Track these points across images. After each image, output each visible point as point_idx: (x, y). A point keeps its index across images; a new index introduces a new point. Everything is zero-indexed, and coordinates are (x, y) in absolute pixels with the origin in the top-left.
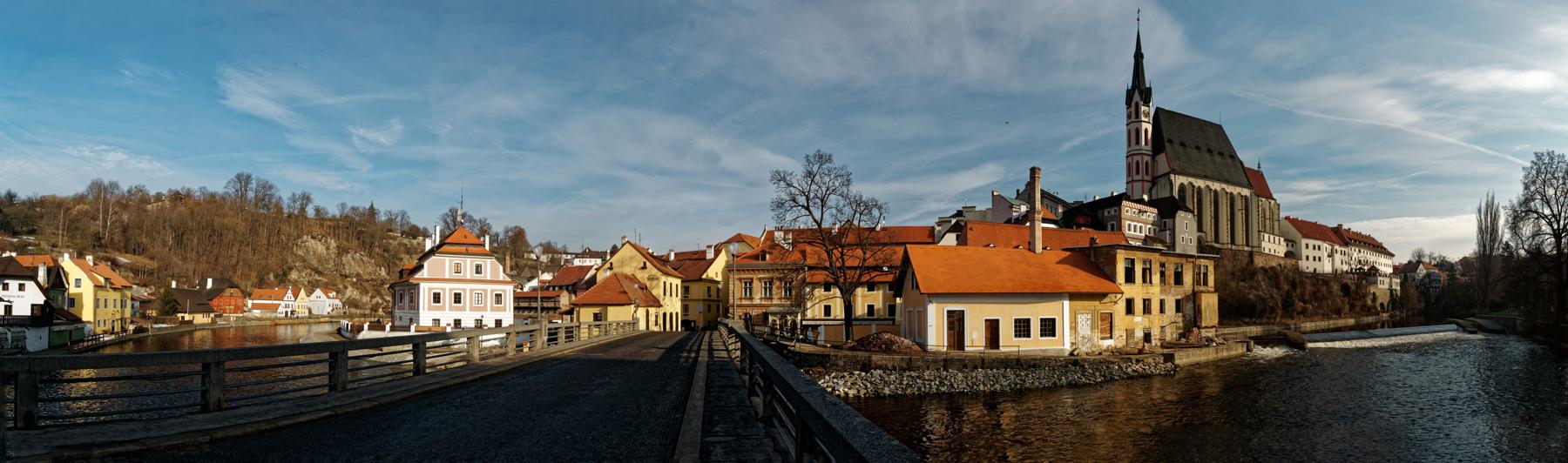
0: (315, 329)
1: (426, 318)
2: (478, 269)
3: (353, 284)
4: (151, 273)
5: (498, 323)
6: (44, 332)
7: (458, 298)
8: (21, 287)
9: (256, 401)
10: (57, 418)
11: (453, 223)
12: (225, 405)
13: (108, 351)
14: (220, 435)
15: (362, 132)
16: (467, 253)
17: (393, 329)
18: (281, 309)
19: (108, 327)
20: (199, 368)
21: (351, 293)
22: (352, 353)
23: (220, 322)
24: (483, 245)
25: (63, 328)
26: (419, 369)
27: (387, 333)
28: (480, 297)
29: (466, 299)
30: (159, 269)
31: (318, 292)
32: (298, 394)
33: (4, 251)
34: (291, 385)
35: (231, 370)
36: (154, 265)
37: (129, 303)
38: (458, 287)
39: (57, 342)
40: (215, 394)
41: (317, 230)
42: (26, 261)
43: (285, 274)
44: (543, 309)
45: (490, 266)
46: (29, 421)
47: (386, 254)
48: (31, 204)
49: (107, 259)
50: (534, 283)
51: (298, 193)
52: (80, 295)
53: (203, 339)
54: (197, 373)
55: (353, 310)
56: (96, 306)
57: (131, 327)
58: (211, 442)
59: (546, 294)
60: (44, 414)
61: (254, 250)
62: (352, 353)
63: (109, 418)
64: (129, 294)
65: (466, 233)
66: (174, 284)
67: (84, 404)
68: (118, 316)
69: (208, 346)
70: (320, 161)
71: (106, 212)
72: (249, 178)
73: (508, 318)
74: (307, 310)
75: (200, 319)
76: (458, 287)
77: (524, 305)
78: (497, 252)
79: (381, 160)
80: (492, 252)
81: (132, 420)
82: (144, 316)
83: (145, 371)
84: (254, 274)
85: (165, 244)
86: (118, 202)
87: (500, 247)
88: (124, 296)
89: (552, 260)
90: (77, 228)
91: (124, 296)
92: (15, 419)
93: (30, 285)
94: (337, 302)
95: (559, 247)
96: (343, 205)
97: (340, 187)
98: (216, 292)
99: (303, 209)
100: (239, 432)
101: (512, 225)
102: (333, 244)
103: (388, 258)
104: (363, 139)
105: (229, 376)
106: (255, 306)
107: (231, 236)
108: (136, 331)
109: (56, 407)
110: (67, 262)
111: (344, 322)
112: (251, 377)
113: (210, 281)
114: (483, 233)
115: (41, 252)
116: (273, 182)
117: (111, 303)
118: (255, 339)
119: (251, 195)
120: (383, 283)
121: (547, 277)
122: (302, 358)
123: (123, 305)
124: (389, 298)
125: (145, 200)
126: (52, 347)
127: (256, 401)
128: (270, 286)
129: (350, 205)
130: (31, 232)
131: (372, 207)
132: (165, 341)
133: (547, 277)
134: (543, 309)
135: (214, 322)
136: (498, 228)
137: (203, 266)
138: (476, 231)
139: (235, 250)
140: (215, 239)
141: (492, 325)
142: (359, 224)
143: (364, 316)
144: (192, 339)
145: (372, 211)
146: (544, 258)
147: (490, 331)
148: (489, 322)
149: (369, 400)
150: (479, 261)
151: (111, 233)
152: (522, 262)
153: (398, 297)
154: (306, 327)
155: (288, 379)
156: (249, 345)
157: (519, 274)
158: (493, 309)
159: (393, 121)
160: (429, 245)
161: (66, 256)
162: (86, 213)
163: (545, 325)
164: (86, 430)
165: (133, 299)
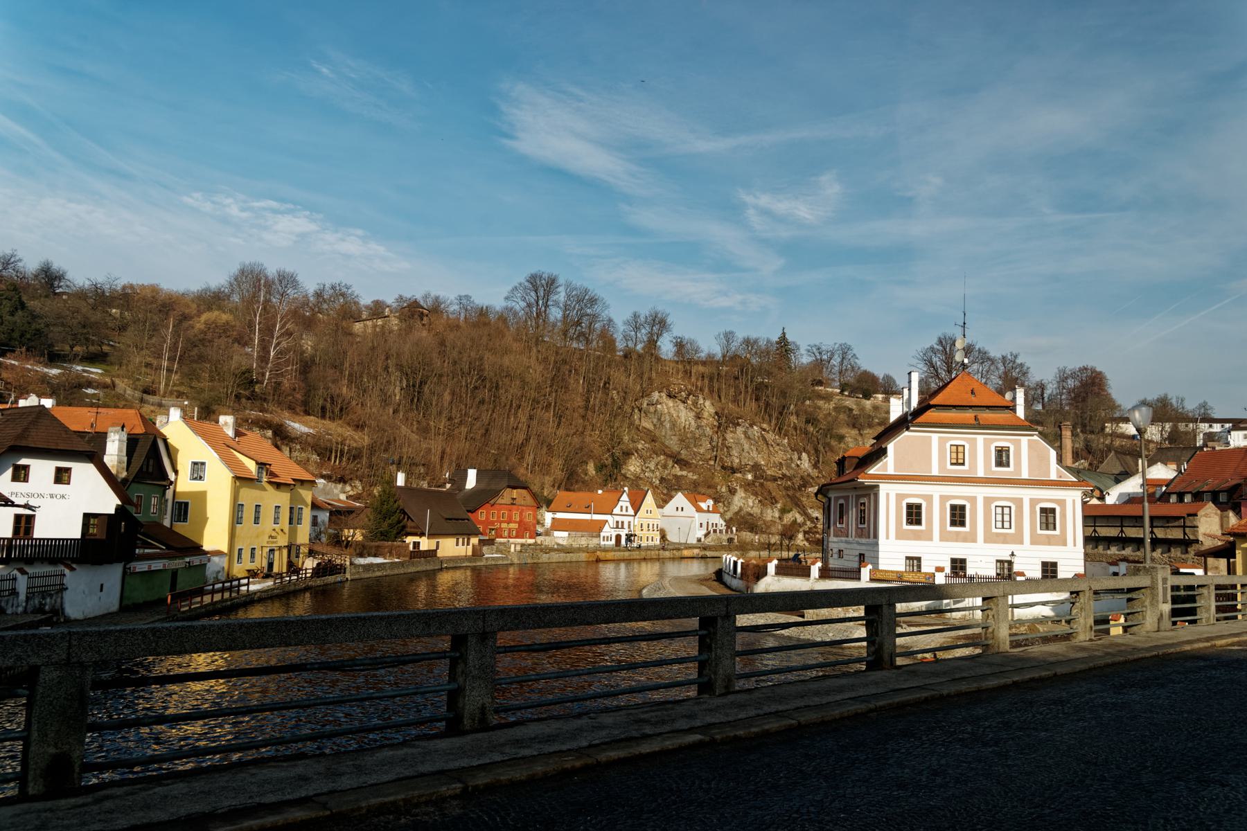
0: (674, 570)
1: (893, 553)
2: (1002, 457)
3: (748, 486)
4: (356, 456)
5: (1049, 569)
6: (112, 576)
7: (958, 516)
8: (62, 476)
9: (557, 710)
10: (130, 764)
11: (944, 367)
12: (494, 720)
13: (256, 613)
14: (482, 780)
15: (764, 200)
16: (978, 425)
17: (825, 574)
18: (608, 531)
19: (260, 563)
20: (445, 644)
21: (743, 501)
22: (743, 620)
23: (489, 554)
24: (1012, 408)
25: (157, 565)
26: (880, 653)
27: (813, 582)
28: (1006, 515)
29: (977, 517)
30: (372, 449)
31: (680, 499)
32: (638, 699)
33: (24, 393)
34: (624, 679)
35: (508, 650)
36: (362, 439)
37: (307, 514)
38: (959, 494)
39: (141, 594)
40: (475, 698)
41: (678, 382)
42: (77, 419)
43: (617, 464)
44: (1156, 542)
45: (1028, 451)
46: (57, 778)
47: (813, 428)
48: (100, 298)
49: (264, 425)
50: (1133, 486)
51: (644, 312)
52: (201, 496)
53: (454, 589)
54: (441, 655)
55: (747, 536)
56: (237, 516)
57: (310, 564)
58: (465, 795)
59: (1163, 510)
60: (99, 758)
61: (559, 417)
62: (743, 620)
63: (251, 755)
64: (307, 495)
65: (975, 384)
66: (401, 480)
67: (196, 728)
68: (283, 541)
69: (464, 601)
70: (685, 254)
71: (268, 330)
72: (551, 283)
73: (1071, 561)
74: (656, 534)
75: (450, 547)
76: (959, 494)
77: (1107, 532)
78: (1045, 421)
79: (800, 252)
80: (1033, 422)
81: (302, 756)
82: (338, 542)
83: (335, 653)
84: (557, 463)
85: (385, 400)
86: (295, 314)
87: (1048, 412)
88: (295, 499)
89: (1174, 437)
90: (201, 358)
91: (295, 499)
92: (21, 778)
93: (83, 472)
94: (716, 519)
95: (1190, 406)
96: (728, 336)
97: (724, 302)
98: (483, 497)
99: (652, 343)
100: (519, 774)
101: (1074, 364)
102: (709, 408)
103: (816, 434)
104: (765, 212)
105: (505, 663)
106: (558, 525)
107: (515, 389)
108: (319, 571)
109: (128, 742)
110: (175, 427)
111: (729, 558)
112: (547, 664)
113: (472, 475)
114: (1010, 383)
115: (113, 399)
116: (597, 290)
117: (267, 515)
118: (556, 588)
119: (555, 314)
120: (805, 483)
121: (1162, 472)
122: (646, 626)
123: (294, 519)
124: (817, 514)
125: (350, 312)
126: (127, 607)
127: (557, 710)
128: (588, 486)
129: (740, 335)
130: (92, 359)
131: (783, 339)
132: (378, 592)
133: (1162, 472)
134: (1156, 542)
135: (477, 554)
136: (1044, 371)
137: (461, 446)
138: (995, 380)
139: (523, 417)
140: (485, 394)
141: (1037, 573)
142: (759, 370)
143: (769, 547)
144: (433, 587)
145: (784, 347)
146: (1154, 433)
147: (1031, 585)
148: (1028, 565)
149: (777, 714)
150: (1002, 440)
151: (277, 372)
152: (1099, 442)
153: (834, 512)
154: (656, 567)
155: (619, 667)
156: (544, 599)
157: (1093, 468)
158: (1035, 541)
159: (825, 178)
160: (896, 409)
161: (175, 414)
162: (225, 329)
163: (1164, 579)
164: (198, 785)
165: (315, 506)
